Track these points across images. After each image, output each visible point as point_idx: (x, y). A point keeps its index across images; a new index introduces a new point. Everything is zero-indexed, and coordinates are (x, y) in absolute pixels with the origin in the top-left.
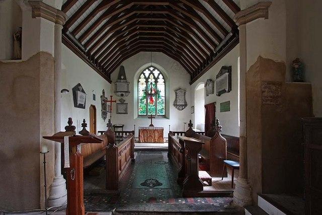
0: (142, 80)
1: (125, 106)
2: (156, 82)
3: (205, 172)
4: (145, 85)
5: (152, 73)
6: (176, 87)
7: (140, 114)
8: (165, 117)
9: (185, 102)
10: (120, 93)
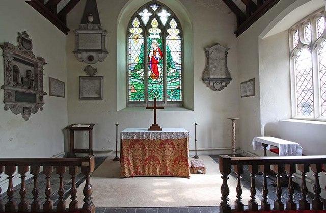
0: (136, 31)
1: (97, 82)
2: (164, 34)
4: (141, 41)
5: (155, 16)
6: (208, 40)
8: (185, 104)
9: (228, 73)
10: (85, 55)
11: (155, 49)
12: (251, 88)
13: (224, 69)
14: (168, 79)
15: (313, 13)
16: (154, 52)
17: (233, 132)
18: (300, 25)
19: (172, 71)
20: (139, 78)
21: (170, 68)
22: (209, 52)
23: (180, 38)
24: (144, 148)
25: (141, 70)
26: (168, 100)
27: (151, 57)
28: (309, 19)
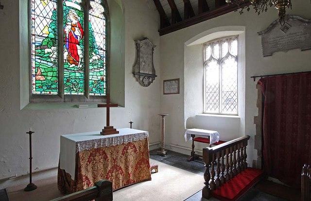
3: (202, 196)
7: (34, 92)
9: (154, 70)
11: (75, 22)
12: (176, 86)
13: (151, 65)
14: (91, 67)
15: (221, 38)
16: (72, 26)
17: (163, 128)
18: (212, 43)
19: (95, 57)
20: (49, 60)
21: (93, 53)
22: (139, 44)
23: (104, 18)
24: (106, 158)
25: (53, 48)
26: (90, 94)
27: (67, 33)
28: (218, 41)
